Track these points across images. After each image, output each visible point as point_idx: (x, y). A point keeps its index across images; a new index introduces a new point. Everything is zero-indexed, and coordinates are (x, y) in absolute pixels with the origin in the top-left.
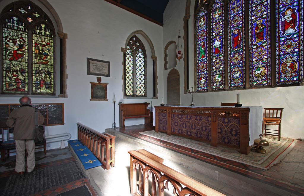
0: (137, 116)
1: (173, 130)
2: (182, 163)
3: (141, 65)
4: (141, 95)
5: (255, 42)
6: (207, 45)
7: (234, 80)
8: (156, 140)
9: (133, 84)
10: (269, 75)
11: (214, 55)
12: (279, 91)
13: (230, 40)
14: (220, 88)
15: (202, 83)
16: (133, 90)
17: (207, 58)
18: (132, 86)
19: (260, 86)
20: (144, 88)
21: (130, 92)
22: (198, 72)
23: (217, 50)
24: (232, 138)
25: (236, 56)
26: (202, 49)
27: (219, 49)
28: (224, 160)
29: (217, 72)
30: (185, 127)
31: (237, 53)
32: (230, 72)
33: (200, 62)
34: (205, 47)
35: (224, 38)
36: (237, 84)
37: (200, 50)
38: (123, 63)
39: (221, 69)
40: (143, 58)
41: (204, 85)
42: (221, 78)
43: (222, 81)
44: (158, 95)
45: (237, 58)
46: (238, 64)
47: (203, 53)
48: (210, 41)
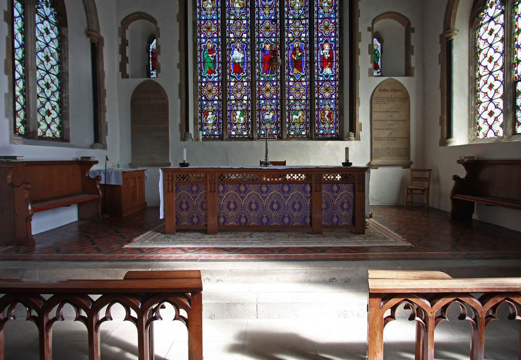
0: (65, 200)
1: (222, 220)
2: (334, 277)
3: (51, 44)
4: (51, 136)
5: (292, 72)
6: (218, 51)
7: (264, 124)
8: (208, 251)
9: (24, 97)
10: (308, 123)
11: (232, 75)
12: (329, 146)
13: (259, 57)
14: (242, 135)
15: (209, 122)
16: (25, 116)
17: (218, 76)
18: (23, 103)
19: (298, 137)
20: (58, 116)
21: (493, 127)
22: (201, 100)
23: (238, 68)
24: (273, 214)
25: (268, 85)
26: (210, 55)
27: (242, 66)
28: (283, 250)
29: (237, 106)
30: (186, 210)
31: (268, 81)
32: (260, 110)
33: (204, 80)
34: (215, 54)
35: (251, 47)
36: (210, 131)
37: (205, 57)
38: (6, 13)
39: (245, 102)
40: (56, 25)
41: (214, 127)
42: (245, 118)
43: (246, 123)
44: (109, 140)
45: (269, 89)
46: (270, 99)
47: (211, 65)
48: (225, 47)
